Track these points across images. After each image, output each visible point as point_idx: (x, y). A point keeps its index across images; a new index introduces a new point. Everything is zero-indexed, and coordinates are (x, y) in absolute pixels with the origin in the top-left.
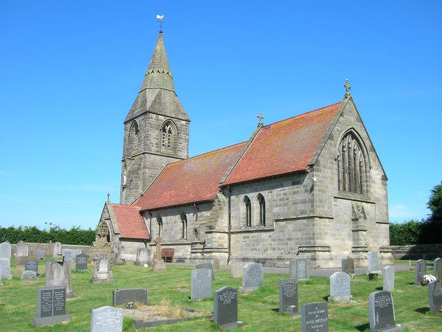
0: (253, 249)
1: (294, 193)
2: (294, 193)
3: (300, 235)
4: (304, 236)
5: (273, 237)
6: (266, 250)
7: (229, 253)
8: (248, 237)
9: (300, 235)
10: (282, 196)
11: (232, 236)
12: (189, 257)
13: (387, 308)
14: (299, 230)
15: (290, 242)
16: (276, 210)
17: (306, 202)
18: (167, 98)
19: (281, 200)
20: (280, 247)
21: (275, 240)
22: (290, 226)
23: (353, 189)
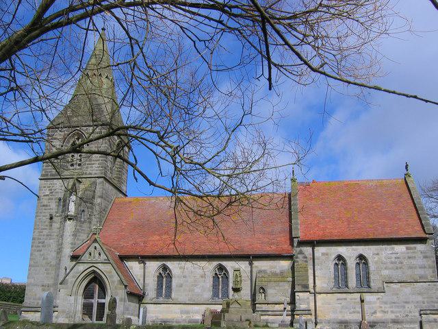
0: (354, 312)
1: (409, 258)
2: (409, 258)
3: (420, 298)
4: (426, 300)
5: (384, 300)
6: (375, 312)
7: (293, 316)
8: (345, 299)
9: (420, 298)
10: (393, 260)
11: (318, 296)
12: (235, 100)
13: (141, 296)
14: (419, 294)
15: (407, 306)
16: (385, 273)
17: (425, 267)
18: (109, 164)
19: (392, 263)
20: (394, 310)
21: (386, 303)
22: (407, 289)
23: (353, 281)
